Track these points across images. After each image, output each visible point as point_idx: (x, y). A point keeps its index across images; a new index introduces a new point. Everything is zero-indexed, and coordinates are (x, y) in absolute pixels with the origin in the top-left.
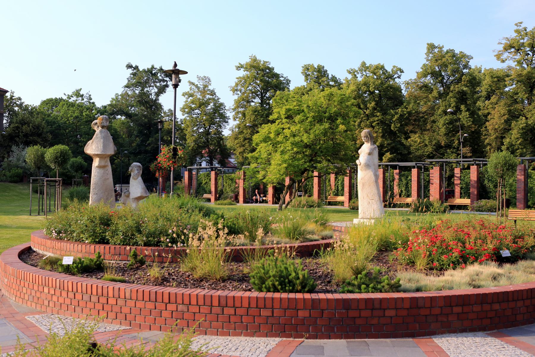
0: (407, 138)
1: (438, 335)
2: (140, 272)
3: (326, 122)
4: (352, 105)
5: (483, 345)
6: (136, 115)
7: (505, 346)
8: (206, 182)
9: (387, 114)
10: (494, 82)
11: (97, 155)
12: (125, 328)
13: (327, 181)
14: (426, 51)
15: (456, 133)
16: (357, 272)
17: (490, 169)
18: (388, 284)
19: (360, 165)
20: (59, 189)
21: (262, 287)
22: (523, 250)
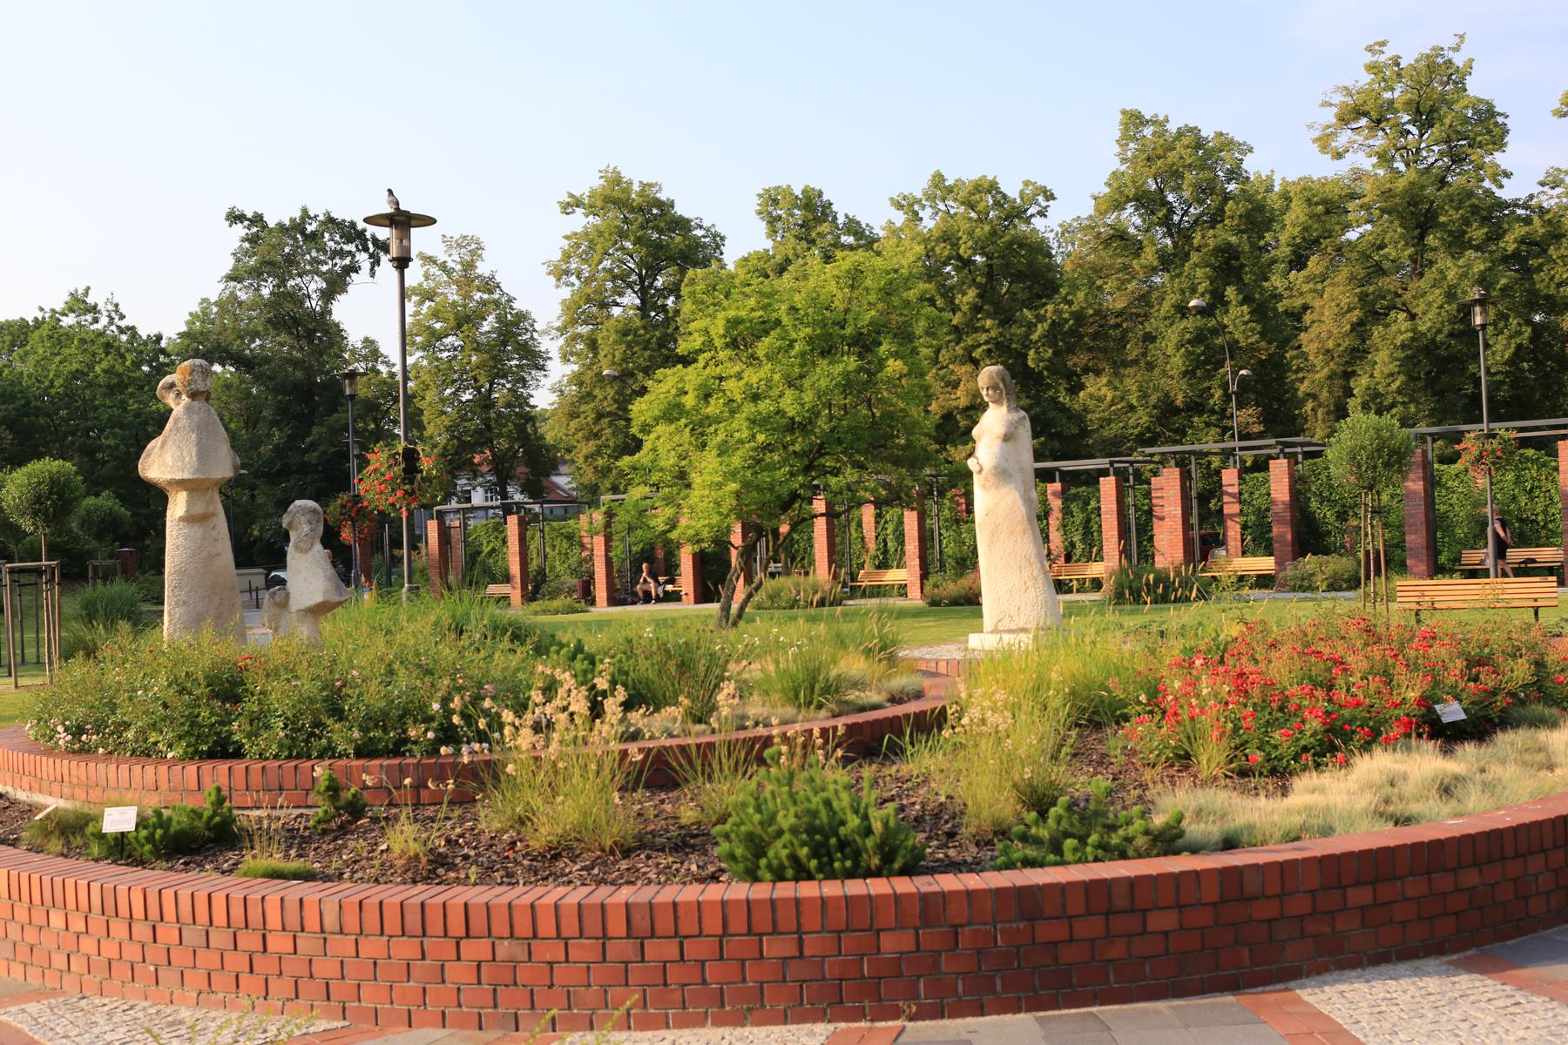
0: (1075, 389)
1: (1308, 976)
2: (357, 844)
4: (922, 299)
5: (1453, 1001)
6: (267, 360)
7: (1519, 997)
8: (493, 550)
9: (1015, 322)
10: (1316, 215)
11: (182, 484)
12: (329, 1026)
14: (1118, 135)
15: (1216, 369)
18: (1147, 832)
19: (980, 471)
20: (53, 596)
21: (758, 867)
22: (1499, 698)
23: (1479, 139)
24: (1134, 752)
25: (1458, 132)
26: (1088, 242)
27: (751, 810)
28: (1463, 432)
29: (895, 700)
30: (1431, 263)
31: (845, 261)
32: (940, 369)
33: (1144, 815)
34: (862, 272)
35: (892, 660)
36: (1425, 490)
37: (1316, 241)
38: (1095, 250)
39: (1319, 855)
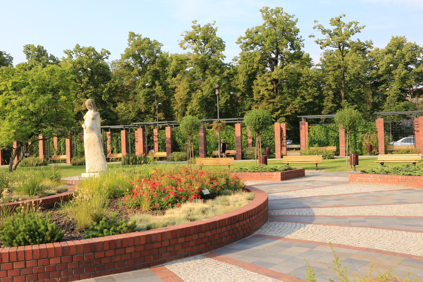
0: (115, 106)
1: (168, 262)
3: (50, 93)
4: (71, 79)
5: (203, 265)
9: (99, 87)
10: (179, 64)
13: (51, 143)
14: (128, 38)
15: (153, 102)
16: (98, 219)
17: (182, 129)
18: (126, 226)
21: (13, 242)
22: (218, 188)
23: (218, 47)
24: (125, 205)
25: (214, 45)
26: (119, 67)
27: (11, 226)
28: (213, 121)
29: (59, 192)
30: (207, 78)
31: (49, 67)
32: (77, 99)
33: (126, 222)
34: (54, 71)
35: (58, 181)
36: (204, 135)
37: (179, 70)
38: (121, 69)
39: (171, 230)
